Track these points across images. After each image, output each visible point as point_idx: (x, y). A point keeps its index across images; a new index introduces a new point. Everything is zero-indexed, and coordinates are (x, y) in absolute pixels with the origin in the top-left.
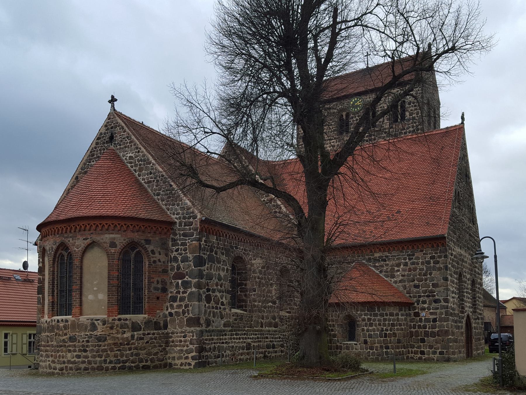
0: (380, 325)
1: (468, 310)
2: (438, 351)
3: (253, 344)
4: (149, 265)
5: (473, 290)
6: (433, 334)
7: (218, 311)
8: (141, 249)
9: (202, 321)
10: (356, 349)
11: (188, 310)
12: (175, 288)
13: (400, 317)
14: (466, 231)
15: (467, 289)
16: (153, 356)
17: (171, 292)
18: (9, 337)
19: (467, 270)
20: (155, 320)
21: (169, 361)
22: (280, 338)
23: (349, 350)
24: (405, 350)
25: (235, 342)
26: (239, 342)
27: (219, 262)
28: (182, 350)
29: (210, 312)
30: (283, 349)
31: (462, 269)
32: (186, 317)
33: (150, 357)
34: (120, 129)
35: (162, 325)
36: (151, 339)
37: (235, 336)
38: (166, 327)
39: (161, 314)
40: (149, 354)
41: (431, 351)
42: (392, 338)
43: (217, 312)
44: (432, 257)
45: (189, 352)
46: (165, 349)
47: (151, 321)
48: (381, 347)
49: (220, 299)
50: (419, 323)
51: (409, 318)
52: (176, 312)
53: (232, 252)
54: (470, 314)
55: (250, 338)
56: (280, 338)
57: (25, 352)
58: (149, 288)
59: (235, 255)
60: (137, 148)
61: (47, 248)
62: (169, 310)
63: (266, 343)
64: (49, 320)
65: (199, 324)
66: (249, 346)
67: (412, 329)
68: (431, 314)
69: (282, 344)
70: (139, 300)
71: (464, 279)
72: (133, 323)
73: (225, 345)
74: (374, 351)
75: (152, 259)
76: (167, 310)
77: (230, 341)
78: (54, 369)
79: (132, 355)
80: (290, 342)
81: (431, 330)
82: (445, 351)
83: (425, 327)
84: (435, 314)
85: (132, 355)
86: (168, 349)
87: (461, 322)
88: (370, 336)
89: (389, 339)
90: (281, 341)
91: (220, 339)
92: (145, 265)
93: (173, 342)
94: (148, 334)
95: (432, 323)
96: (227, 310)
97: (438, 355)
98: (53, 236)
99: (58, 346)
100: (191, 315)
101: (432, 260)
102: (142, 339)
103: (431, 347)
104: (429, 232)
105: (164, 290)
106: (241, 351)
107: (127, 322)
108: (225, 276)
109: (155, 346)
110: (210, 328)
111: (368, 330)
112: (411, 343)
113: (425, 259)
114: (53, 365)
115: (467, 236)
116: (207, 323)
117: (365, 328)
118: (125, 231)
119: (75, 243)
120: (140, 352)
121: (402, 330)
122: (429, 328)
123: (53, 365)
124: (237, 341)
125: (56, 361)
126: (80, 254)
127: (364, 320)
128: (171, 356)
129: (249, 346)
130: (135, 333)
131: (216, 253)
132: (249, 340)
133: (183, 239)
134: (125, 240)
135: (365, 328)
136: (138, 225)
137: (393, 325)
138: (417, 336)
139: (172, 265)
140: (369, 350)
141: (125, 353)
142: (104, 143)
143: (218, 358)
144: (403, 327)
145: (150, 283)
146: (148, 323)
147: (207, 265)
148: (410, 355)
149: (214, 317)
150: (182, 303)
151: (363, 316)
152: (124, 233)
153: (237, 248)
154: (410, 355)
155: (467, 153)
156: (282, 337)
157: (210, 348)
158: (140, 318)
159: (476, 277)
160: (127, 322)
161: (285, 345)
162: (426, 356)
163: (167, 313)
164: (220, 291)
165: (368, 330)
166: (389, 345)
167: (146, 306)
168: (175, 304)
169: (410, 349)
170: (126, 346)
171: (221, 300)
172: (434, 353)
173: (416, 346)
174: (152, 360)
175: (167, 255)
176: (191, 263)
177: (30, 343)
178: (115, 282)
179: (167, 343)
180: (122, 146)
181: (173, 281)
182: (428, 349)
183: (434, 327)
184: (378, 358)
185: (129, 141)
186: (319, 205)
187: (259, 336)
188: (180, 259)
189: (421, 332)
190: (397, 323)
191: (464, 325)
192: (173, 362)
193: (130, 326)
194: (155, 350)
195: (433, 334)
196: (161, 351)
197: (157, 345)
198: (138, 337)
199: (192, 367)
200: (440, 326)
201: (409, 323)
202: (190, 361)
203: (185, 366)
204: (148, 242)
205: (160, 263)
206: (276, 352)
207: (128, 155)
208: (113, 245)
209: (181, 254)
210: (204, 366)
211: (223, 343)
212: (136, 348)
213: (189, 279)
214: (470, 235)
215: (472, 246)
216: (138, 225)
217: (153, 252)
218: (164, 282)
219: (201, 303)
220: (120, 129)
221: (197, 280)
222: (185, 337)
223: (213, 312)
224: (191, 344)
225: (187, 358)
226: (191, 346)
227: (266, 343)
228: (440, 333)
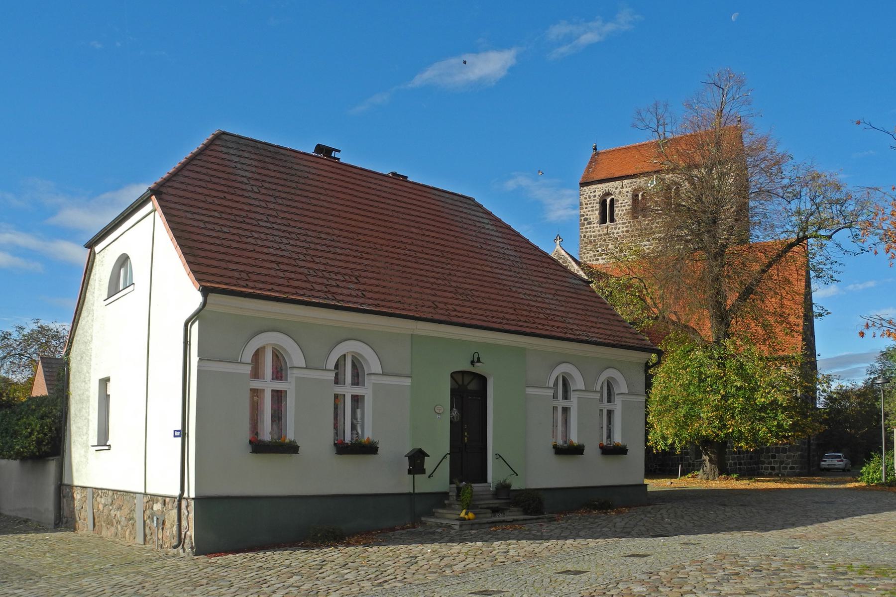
48: (735, 464)
97: (788, 470)
172: (785, 468)
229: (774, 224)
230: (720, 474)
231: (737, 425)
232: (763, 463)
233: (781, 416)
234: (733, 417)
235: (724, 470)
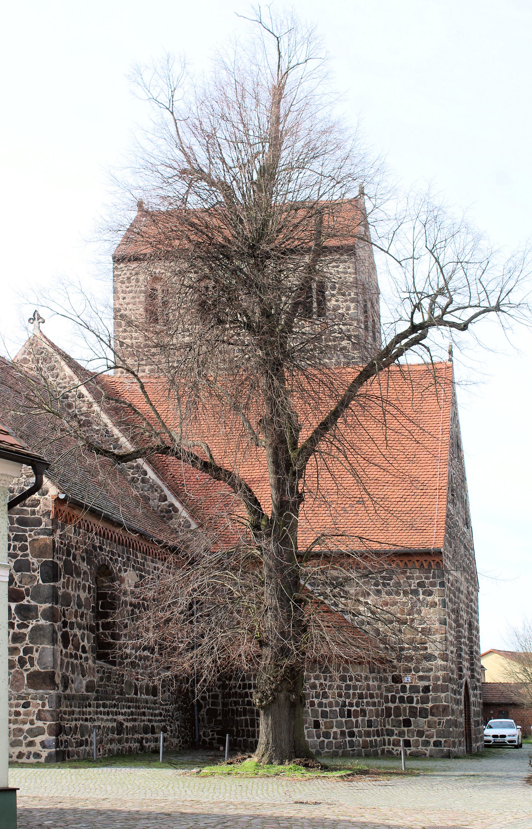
0: (340, 696)
2: (432, 740)
3: (126, 724)
7: (79, 662)
9: (58, 680)
11: (31, 659)
13: (371, 683)
15: (465, 637)
19: (464, 606)
22: (160, 714)
24: (378, 739)
25: (102, 719)
27: (78, 575)
28: (21, 730)
29: (68, 662)
32: (26, 670)
37: (102, 709)
41: (420, 739)
42: (360, 719)
43: (77, 663)
44: (421, 585)
45: (40, 732)
48: (343, 733)
49: (80, 641)
50: (402, 694)
51: (384, 685)
53: (96, 557)
55: (122, 714)
56: (160, 714)
59: (99, 561)
63: (142, 724)
65: (54, 685)
66: (120, 729)
67: (390, 704)
68: (421, 678)
69: (164, 727)
73: (89, 724)
74: (331, 739)
77: (95, 717)
80: (175, 725)
81: (419, 706)
82: (442, 740)
83: (410, 700)
84: (427, 678)
88: (324, 714)
95: (421, 694)
96: (90, 662)
97: (431, 747)
100: (37, 668)
101: (420, 589)
103: (420, 734)
104: (413, 541)
106: (110, 736)
108: (86, 599)
110: (68, 692)
111: (320, 705)
112: (387, 727)
113: (410, 586)
116: (65, 683)
117: (316, 701)
121: (374, 704)
122: (417, 703)
124: (105, 717)
127: (314, 686)
129: (120, 729)
131: (74, 559)
132: (120, 718)
133: (18, 529)
135: (316, 701)
137: (361, 696)
138: (398, 715)
143: (81, 746)
144: (376, 700)
147: (62, 580)
148: (386, 747)
149: (73, 673)
150: (18, 645)
151: (313, 680)
153: (101, 549)
154: (386, 747)
156: (164, 713)
157: (70, 727)
161: (168, 728)
162: (413, 749)
164: (80, 627)
165: (320, 705)
166: (355, 730)
169: (386, 738)
171: (82, 644)
172: (426, 743)
173: (396, 732)
176: (36, 574)
182: (416, 738)
183: (425, 700)
184: (337, 752)
186: (289, 504)
187: (134, 710)
189: (405, 709)
190: (366, 693)
195: (424, 713)
199: (42, 760)
200: (435, 699)
201: (384, 694)
202: (38, 748)
203: (28, 757)
210: (63, 760)
211: (86, 720)
213: (33, 603)
219: (55, 647)
221: (48, 605)
222: (26, 705)
223: (72, 663)
224: (39, 718)
225: (31, 744)
226: (39, 724)
227: (142, 724)
228: (434, 711)
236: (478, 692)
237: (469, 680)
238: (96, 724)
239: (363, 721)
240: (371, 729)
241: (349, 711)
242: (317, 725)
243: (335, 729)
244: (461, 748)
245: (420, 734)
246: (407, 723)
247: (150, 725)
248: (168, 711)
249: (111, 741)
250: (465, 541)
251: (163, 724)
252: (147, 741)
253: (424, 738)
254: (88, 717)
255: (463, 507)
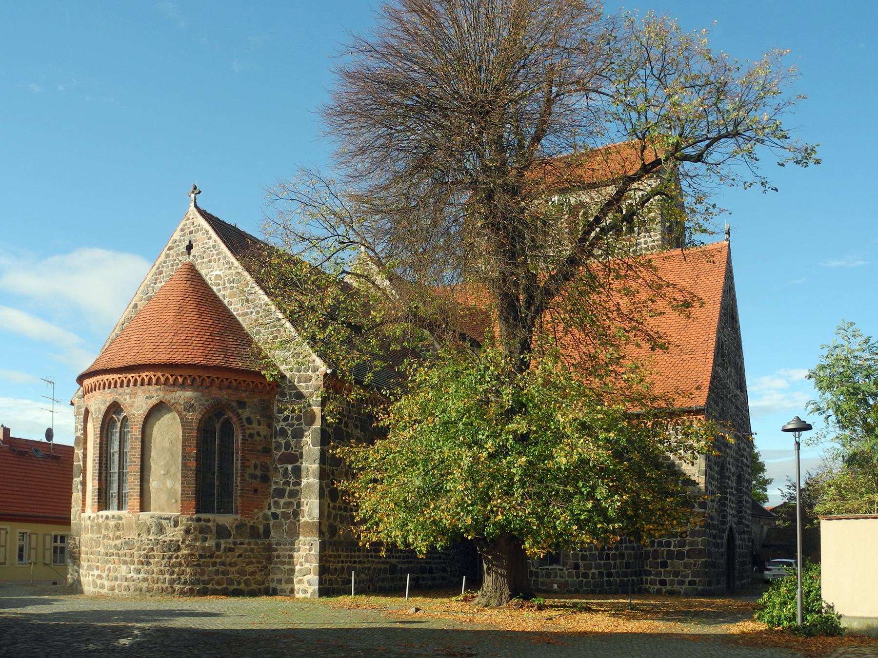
1: (731, 520)
2: (687, 580)
3: (400, 566)
4: (242, 439)
5: (739, 490)
6: (680, 556)
8: (231, 415)
10: (561, 577)
12: (281, 477)
14: (731, 401)
15: (731, 488)
16: (248, 577)
17: (276, 483)
18: (26, 538)
19: (732, 460)
20: (251, 524)
21: (273, 585)
23: (549, 577)
24: (636, 579)
25: (373, 562)
26: (379, 562)
29: (336, 515)
30: (444, 575)
31: (725, 458)
33: (245, 578)
34: (203, 234)
35: (261, 531)
36: (246, 550)
38: (267, 533)
39: (260, 515)
40: (242, 573)
42: (618, 561)
46: (266, 567)
47: (246, 524)
48: (601, 574)
52: (282, 513)
54: (734, 526)
55: (396, 557)
57: (47, 561)
58: (242, 476)
60: (228, 263)
61: (92, 409)
62: (273, 510)
64: (93, 515)
70: (226, 489)
71: (728, 474)
72: (218, 526)
75: (248, 432)
76: (270, 509)
77: (366, 560)
78: (100, 588)
79: (217, 572)
82: (697, 580)
83: (668, 544)
85: (217, 572)
86: (270, 567)
87: (721, 538)
89: (612, 563)
90: (442, 563)
91: (351, 557)
92: (237, 440)
93: (278, 557)
94: (242, 544)
97: (686, 586)
98: (101, 390)
99: (106, 554)
102: (231, 550)
103: (676, 574)
105: (266, 479)
106: (382, 576)
107: (210, 524)
109: (251, 563)
110: (336, 538)
114: (99, 582)
115: (733, 410)
118: (207, 388)
119: (134, 402)
120: (229, 568)
121: (633, 548)
122: (675, 546)
123: (99, 582)
125: (104, 575)
126: (141, 420)
128: (275, 577)
130: (222, 541)
131: (346, 426)
134: (207, 401)
136: (227, 379)
139: (277, 442)
140: (581, 579)
141: (206, 569)
142: (178, 255)
145: (244, 467)
146: (240, 527)
150: (292, 500)
152: (207, 391)
155: (733, 285)
158: (227, 520)
159: (742, 469)
160: (210, 524)
162: (669, 587)
163: (269, 513)
166: (613, 571)
167: (237, 501)
168: (282, 501)
170: (208, 560)
172: (681, 583)
174: (247, 582)
175: (270, 426)
177: (55, 548)
178: (193, 464)
179: (269, 559)
180: (204, 260)
181: (279, 466)
182: (671, 578)
183: (682, 544)
185: (215, 253)
188: (290, 432)
191: (725, 541)
192: (279, 587)
193: (214, 530)
194: (250, 568)
195: (680, 556)
196: (261, 571)
197: (254, 560)
198: (225, 548)
200: (692, 543)
204: (242, 404)
205: (258, 438)
206: (434, 579)
207: (214, 273)
208: (190, 407)
209: (291, 425)
211: (355, 562)
212: (223, 564)
214: (737, 407)
215: (739, 424)
216: (227, 379)
217: (249, 421)
218: (265, 467)
220: (203, 234)
224: (306, 561)
226: (307, 565)
229: (599, 129)
230: (511, 597)
231: (512, 509)
232: (649, 573)
233: (601, 492)
234: (508, 493)
235: (523, 588)
236: (746, 536)
237: (734, 526)
238: (366, 565)
239: (621, 563)
240: (629, 570)
241: (608, 555)
242: (576, 567)
243: (593, 570)
244: (720, 586)
245: (676, 574)
246: (664, 565)
247: (428, 566)
248: (449, 555)
249: (383, 580)
250: (738, 403)
251: (443, 565)
252: (424, 579)
253: (679, 578)
254: (357, 560)
255: (737, 372)
